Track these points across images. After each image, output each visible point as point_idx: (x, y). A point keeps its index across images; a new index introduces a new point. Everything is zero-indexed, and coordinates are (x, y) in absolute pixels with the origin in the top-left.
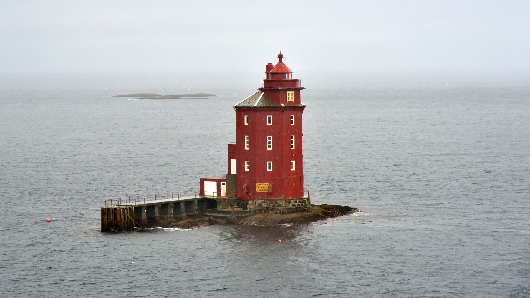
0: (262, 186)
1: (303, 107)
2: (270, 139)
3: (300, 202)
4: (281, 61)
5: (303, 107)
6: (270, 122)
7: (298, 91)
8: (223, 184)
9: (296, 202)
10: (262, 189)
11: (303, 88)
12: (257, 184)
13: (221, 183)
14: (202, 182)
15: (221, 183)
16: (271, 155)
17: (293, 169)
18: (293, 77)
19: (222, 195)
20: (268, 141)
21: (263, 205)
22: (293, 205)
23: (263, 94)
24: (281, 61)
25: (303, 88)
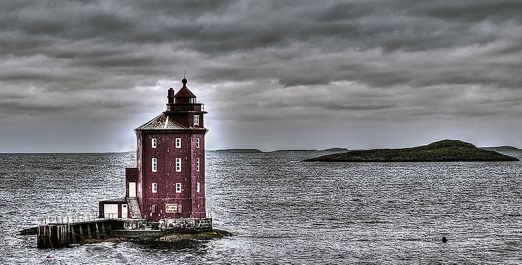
0: (171, 206)
1: (205, 131)
2: (178, 161)
3: (205, 222)
4: (185, 85)
5: (205, 131)
6: (155, 145)
7: (201, 114)
8: (125, 206)
9: (203, 223)
10: (171, 209)
11: (206, 113)
12: (167, 205)
13: (123, 205)
14: (102, 204)
15: (123, 205)
16: (176, 178)
17: (198, 191)
18: (198, 101)
19: (123, 216)
20: (177, 163)
21: (174, 224)
22: (201, 225)
23: (168, 117)
24: (185, 85)
25: (206, 113)
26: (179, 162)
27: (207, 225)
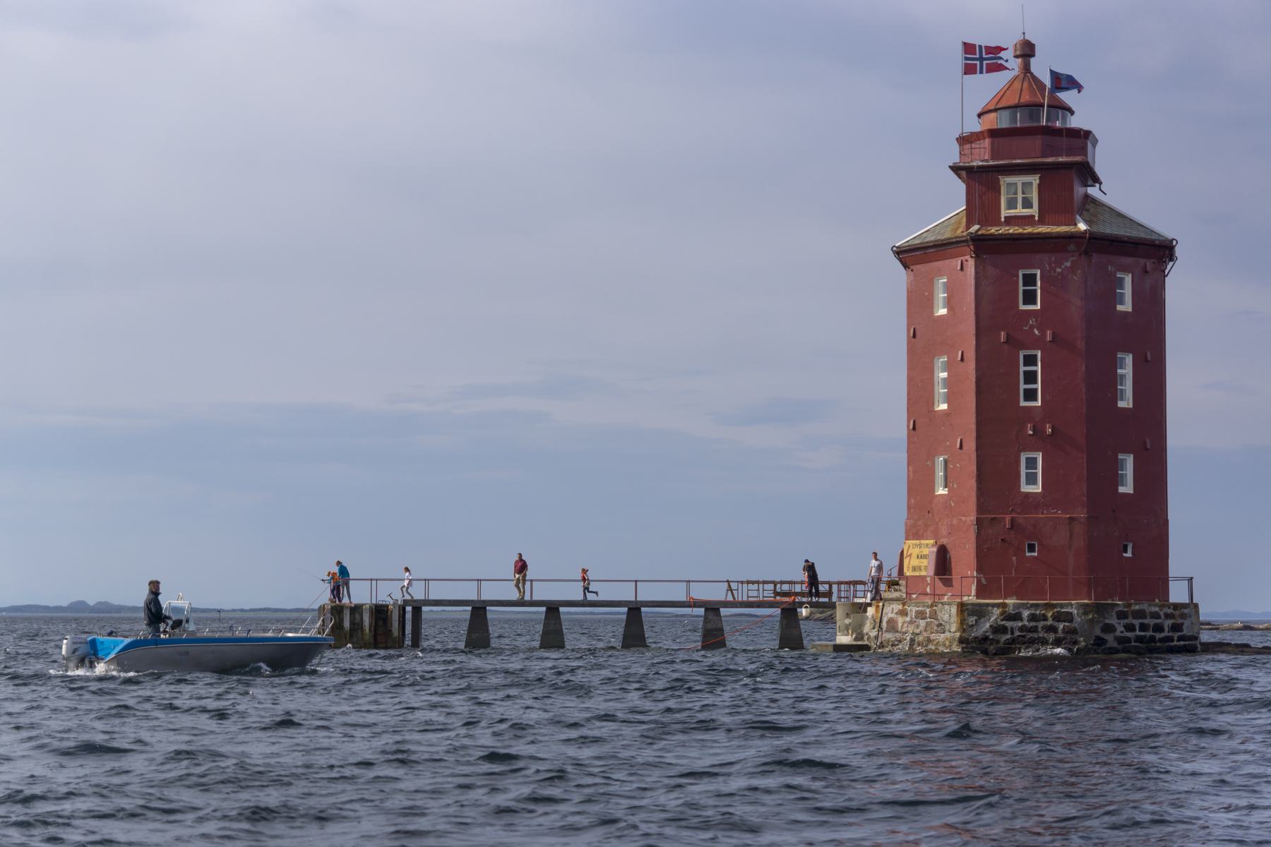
3: (1033, 618)
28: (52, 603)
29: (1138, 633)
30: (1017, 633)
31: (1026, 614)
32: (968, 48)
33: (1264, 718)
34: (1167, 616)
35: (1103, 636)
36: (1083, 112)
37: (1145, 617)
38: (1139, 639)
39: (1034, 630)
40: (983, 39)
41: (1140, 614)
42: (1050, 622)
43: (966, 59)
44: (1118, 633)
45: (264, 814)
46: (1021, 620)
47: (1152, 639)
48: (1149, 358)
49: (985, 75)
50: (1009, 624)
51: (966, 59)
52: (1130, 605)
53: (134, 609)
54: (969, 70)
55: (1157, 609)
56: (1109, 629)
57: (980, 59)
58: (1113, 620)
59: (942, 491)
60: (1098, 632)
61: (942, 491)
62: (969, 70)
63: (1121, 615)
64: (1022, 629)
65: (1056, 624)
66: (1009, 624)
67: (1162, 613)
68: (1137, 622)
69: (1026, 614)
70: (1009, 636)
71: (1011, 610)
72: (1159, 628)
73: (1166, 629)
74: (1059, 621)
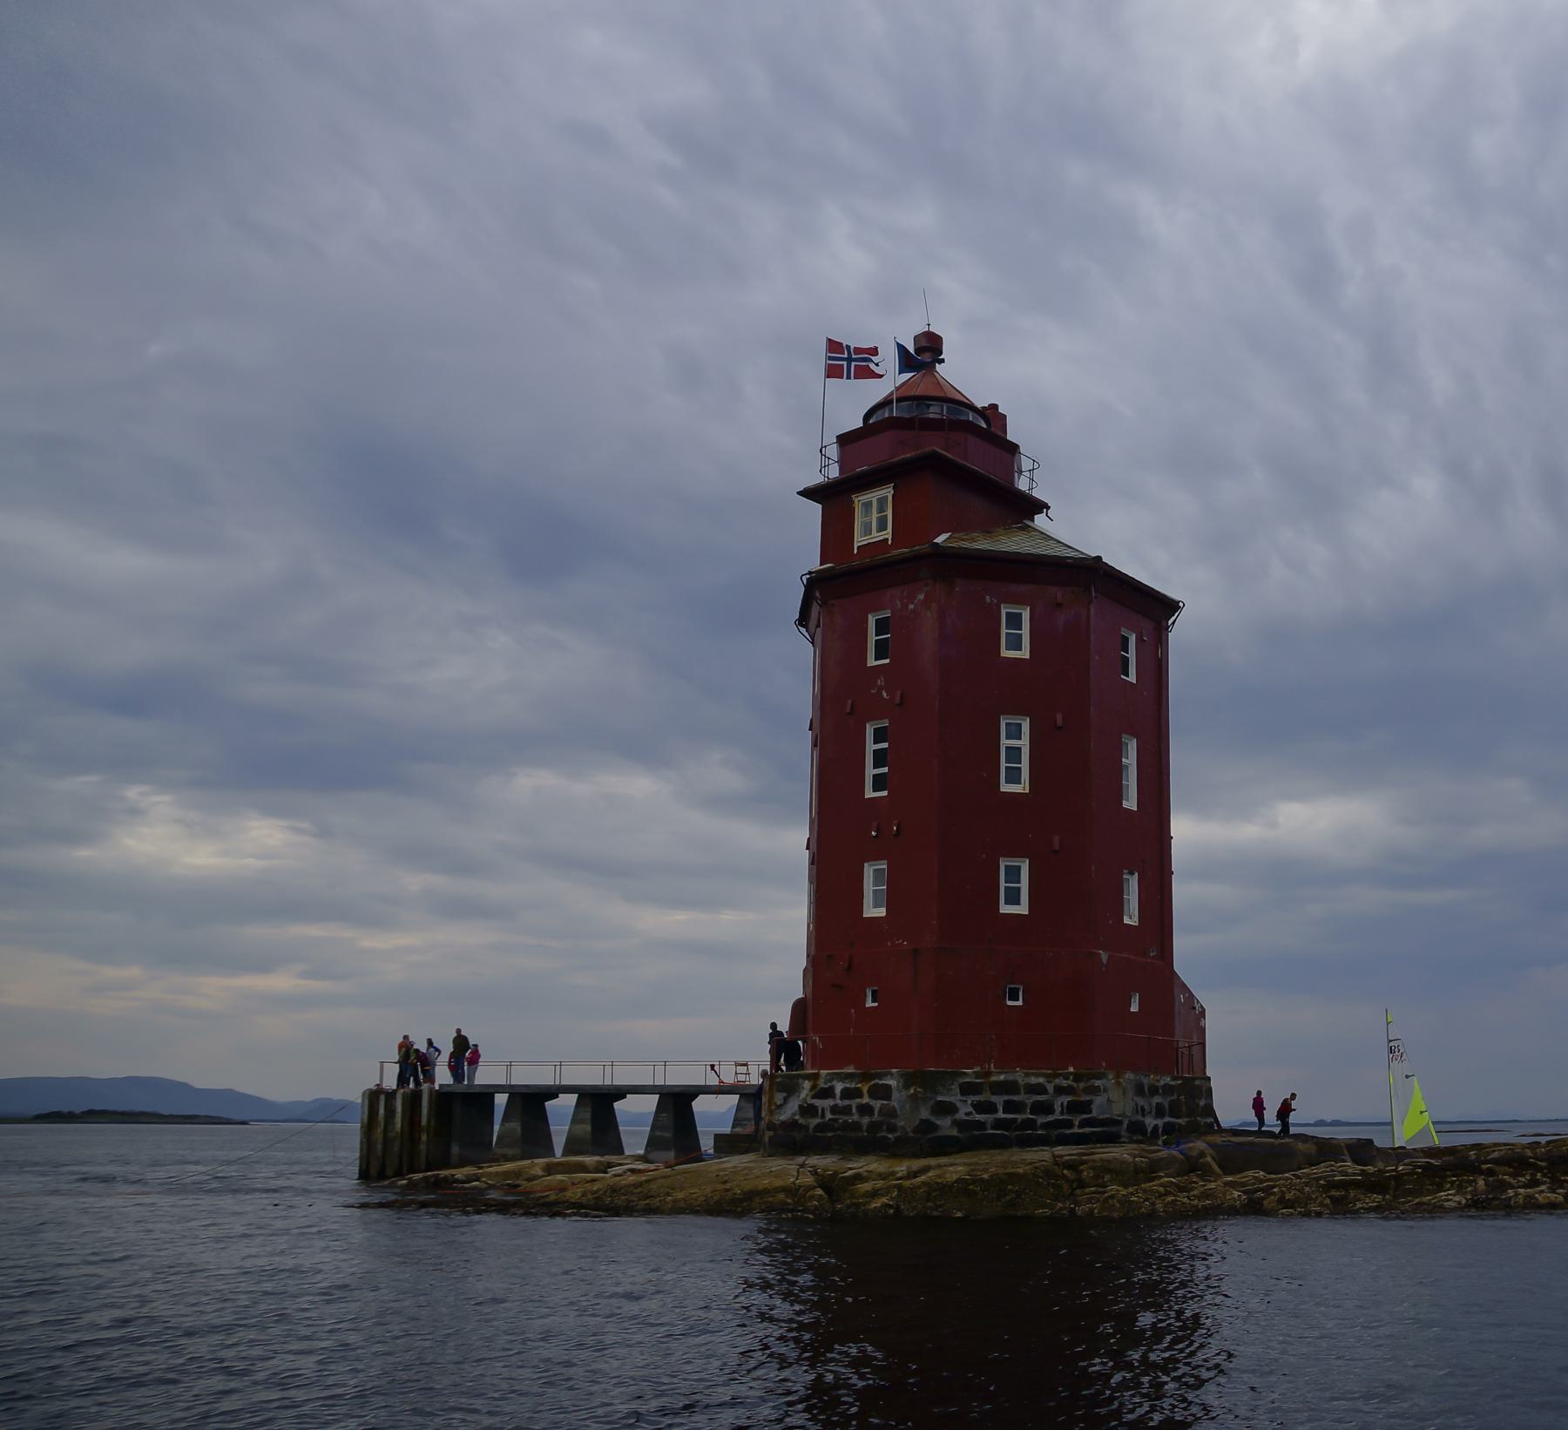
3: (846, 1094)
9: (828, 1093)
26: (1017, 739)
27: (865, 1110)
28: (200, 1083)
29: (1001, 1115)
30: (829, 1116)
31: (839, 1087)
32: (834, 346)
33: (107, 575)
34: (1060, 1090)
35: (933, 1119)
36: (968, 374)
37: (1017, 1092)
38: (999, 1124)
39: (847, 1110)
40: (854, 339)
41: (1009, 1087)
42: (866, 1100)
43: (831, 358)
44: (961, 1116)
45: (338, 1294)
46: (834, 1097)
47: (1030, 1124)
48: (1059, 721)
49: (853, 381)
50: (818, 1103)
51: (831, 358)
52: (988, 1074)
53: (344, 1106)
54: (833, 372)
55: (1041, 1080)
56: (947, 1109)
57: (847, 361)
58: (953, 1096)
59: (870, 1004)
60: (925, 1113)
61: (870, 1004)
62: (833, 372)
63: (967, 1089)
64: (834, 1109)
65: (873, 1103)
66: (818, 1103)
67: (1050, 1088)
68: (999, 1100)
69: (839, 1087)
70: (818, 1120)
71: (822, 1084)
72: (1046, 1108)
73: (1058, 1108)
74: (877, 1098)
